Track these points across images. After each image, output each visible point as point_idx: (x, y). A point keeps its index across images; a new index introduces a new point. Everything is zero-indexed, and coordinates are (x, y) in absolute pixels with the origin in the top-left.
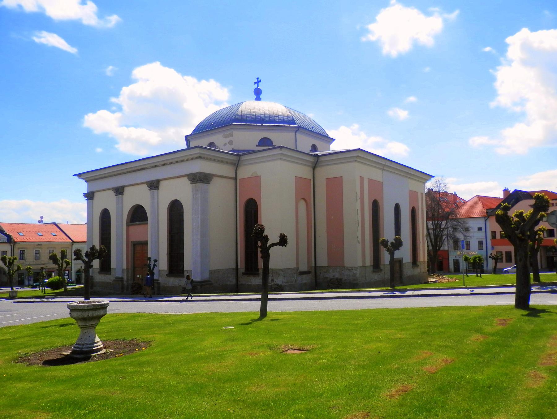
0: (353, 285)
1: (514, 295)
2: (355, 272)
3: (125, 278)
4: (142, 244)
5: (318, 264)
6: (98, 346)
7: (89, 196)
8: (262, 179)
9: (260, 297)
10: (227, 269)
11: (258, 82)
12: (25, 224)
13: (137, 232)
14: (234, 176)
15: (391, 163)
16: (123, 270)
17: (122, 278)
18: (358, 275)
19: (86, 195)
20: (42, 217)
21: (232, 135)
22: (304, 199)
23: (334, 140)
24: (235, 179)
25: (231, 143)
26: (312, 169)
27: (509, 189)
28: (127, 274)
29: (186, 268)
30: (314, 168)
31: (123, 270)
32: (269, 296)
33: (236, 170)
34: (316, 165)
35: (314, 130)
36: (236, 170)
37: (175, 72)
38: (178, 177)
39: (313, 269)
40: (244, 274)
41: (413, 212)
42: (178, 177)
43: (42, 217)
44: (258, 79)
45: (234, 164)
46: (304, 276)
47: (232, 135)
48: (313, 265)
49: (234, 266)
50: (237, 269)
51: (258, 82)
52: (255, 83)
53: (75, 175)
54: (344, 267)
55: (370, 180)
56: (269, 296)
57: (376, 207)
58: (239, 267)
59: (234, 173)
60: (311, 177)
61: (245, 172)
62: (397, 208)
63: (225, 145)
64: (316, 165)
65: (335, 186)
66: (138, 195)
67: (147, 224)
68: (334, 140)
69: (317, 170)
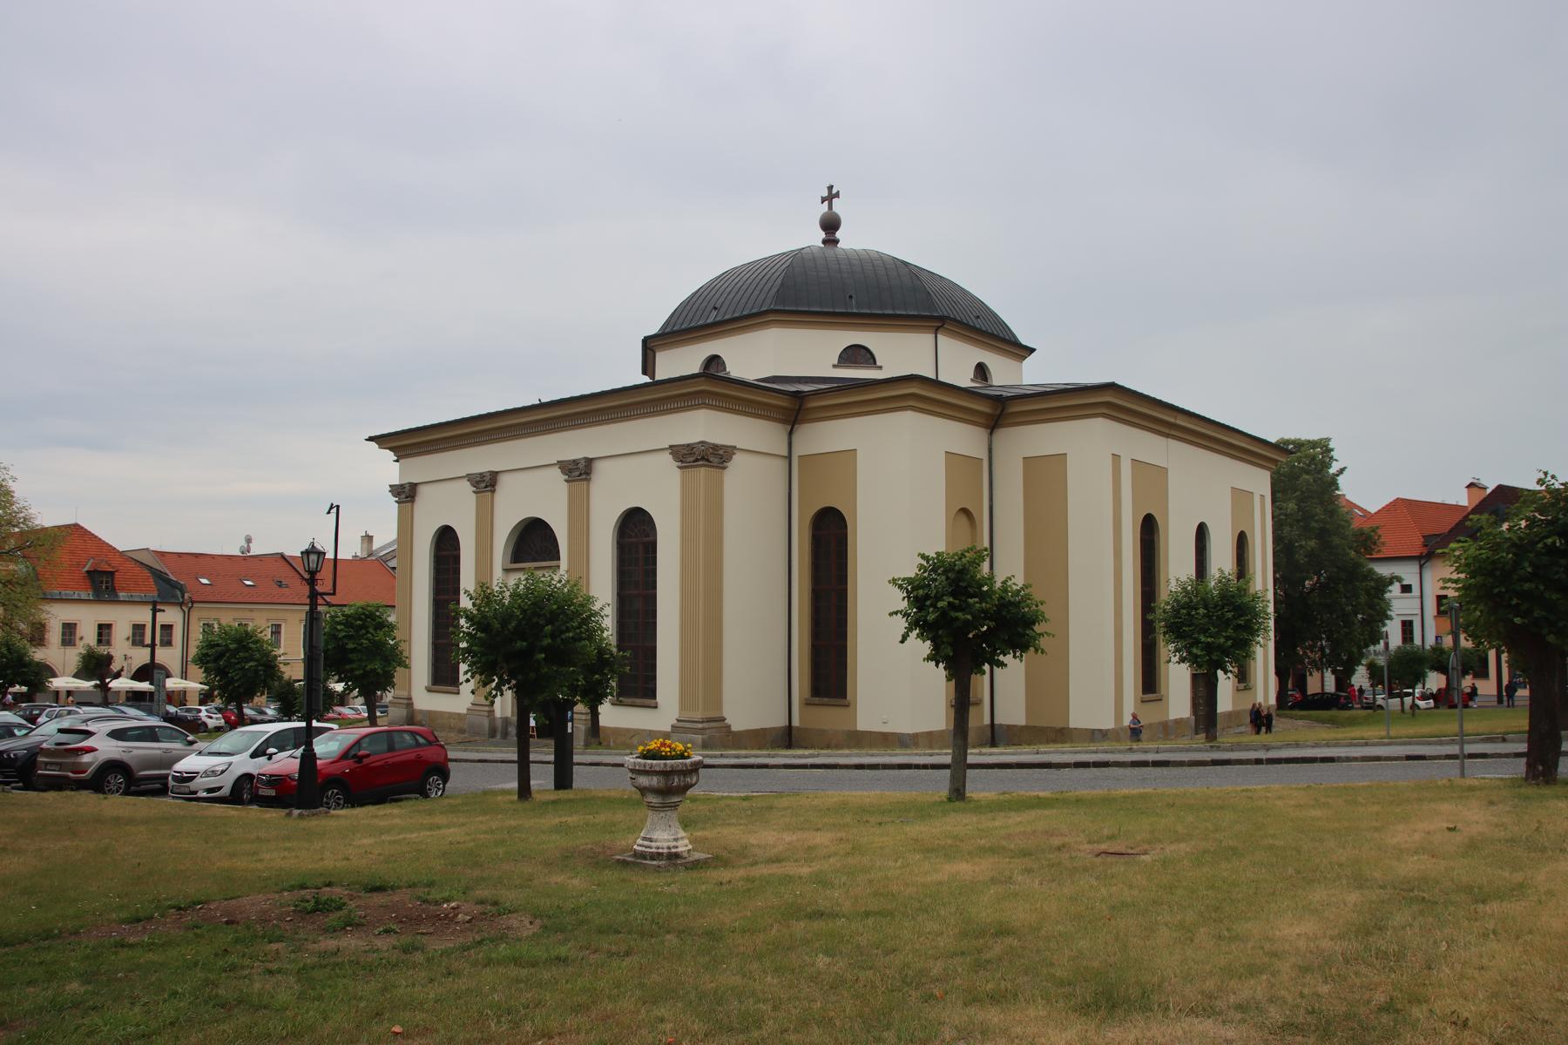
0: (838, 747)
1: (1524, 760)
6: (1242, 542)
7: (406, 494)
9: (948, 760)
11: (831, 196)
12: (213, 557)
19: (397, 490)
20: (249, 540)
23: (1032, 350)
24: (789, 457)
27: (1484, 482)
32: (971, 759)
33: (791, 433)
35: (978, 324)
36: (791, 433)
41: (1242, 542)
43: (249, 540)
44: (830, 188)
51: (831, 196)
53: (371, 439)
57: (1149, 529)
60: (984, 456)
62: (1202, 532)
68: (1032, 350)
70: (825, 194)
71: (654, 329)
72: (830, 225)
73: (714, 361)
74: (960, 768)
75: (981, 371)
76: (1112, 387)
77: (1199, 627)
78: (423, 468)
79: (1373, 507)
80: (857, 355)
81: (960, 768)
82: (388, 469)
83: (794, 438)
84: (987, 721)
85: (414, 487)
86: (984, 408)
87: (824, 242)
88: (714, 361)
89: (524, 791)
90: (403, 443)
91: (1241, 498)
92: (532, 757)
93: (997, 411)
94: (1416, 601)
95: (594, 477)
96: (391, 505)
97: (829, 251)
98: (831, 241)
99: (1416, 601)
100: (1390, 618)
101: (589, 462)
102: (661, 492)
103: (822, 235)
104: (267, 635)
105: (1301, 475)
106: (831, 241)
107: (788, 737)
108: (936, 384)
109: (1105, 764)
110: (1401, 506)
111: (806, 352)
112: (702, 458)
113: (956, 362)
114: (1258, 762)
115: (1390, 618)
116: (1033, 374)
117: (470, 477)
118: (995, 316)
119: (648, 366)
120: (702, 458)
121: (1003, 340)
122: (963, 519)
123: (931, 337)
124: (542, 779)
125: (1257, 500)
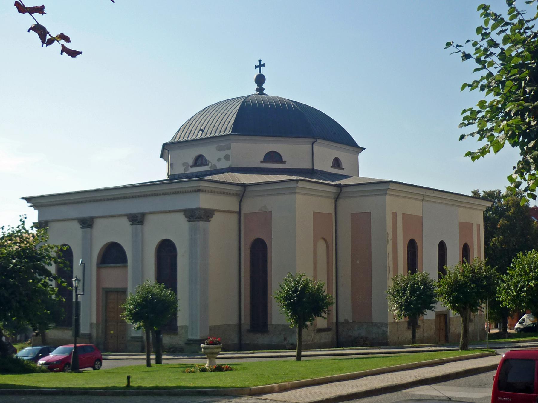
2: (385, 329)
3: (94, 335)
4: (118, 292)
5: (341, 319)
8: (273, 215)
9: (295, 354)
10: (228, 325)
11: (260, 66)
13: (112, 277)
14: (238, 210)
15: (432, 191)
16: (91, 324)
17: (142, 337)
18: (388, 333)
21: (229, 148)
22: (324, 239)
23: (364, 149)
24: (239, 213)
25: (227, 158)
26: (333, 201)
28: (97, 330)
29: (180, 323)
30: (336, 201)
31: (91, 324)
32: (303, 353)
34: (339, 195)
36: (240, 202)
37: (347, 402)
38: (170, 212)
39: (335, 325)
40: (249, 331)
42: (170, 212)
44: (260, 61)
45: (238, 195)
46: (323, 334)
47: (229, 148)
48: (335, 321)
49: (234, 320)
50: (240, 324)
51: (260, 66)
52: (256, 67)
53: (23, 198)
54: (372, 323)
55: (404, 215)
56: (303, 353)
57: (412, 248)
58: (243, 322)
59: (238, 206)
60: (332, 211)
61: (251, 206)
62: (442, 247)
63: (219, 160)
64: (339, 195)
65: (362, 223)
66: (120, 233)
67: (126, 267)
68: (364, 149)
69: (341, 202)
70: (258, 64)
72: (260, 80)
78: (52, 213)
83: (242, 204)
89: (149, 365)
91: (466, 228)
95: (146, 223)
98: (260, 90)
100: (431, 308)
101: (143, 215)
102: (178, 230)
103: (256, 86)
104: (495, 373)
106: (260, 90)
112: (195, 216)
120: (195, 216)
124: (153, 362)
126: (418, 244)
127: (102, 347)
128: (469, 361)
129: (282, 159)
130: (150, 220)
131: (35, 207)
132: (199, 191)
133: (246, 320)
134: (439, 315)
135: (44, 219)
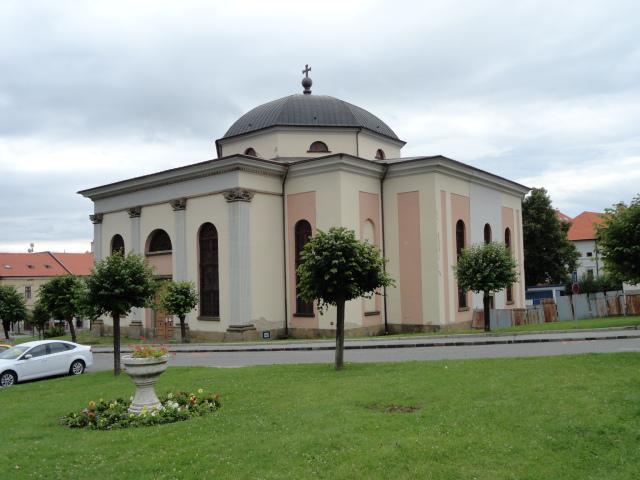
6: (507, 232)
11: (307, 70)
22: (369, 220)
23: (405, 143)
24: (283, 195)
26: (379, 181)
32: (346, 344)
40: (295, 316)
41: (507, 232)
42: (210, 194)
51: (307, 70)
53: (79, 192)
56: (346, 344)
57: (460, 226)
62: (487, 229)
66: (158, 217)
68: (405, 143)
69: (386, 182)
71: (221, 136)
72: (307, 84)
73: (250, 151)
74: (340, 348)
75: (380, 153)
76: (440, 157)
77: (481, 273)
79: (573, 216)
80: (318, 146)
81: (340, 348)
82: (89, 206)
84: (383, 322)
85: (102, 215)
86: (378, 169)
87: (305, 92)
88: (250, 151)
90: (97, 194)
91: (507, 212)
92: (122, 349)
93: (385, 171)
94: (590, 263)
96: (91, 224)
97: (307, 96)
98: (307, 92)
99: (590, 263)
100: (580, 255)
103: (303, 89)
105: (537, 209)
106: (307, 92)
107: (286, 334)
108: (357, 158)
109: (432, 345)
110: (585, 216)
111: (292, 146)
113: (368, 149)
114: (510, 342)
115: (580, 255)
116: (406, 153)
117: (126, 209)
118: (387, 127)
119: (219, 153)
120: (235, 196)
121: (391, 138)
122: (369, 224)
123: (354, 137)
125: (514, 212)
126: (466, 225)
127: (151, 334)
128: (141, 175)
129: (327, 148)
130: (190, 204)
131: (94, 199)
132: (238, 169)
133: (292, 308)
134: (214, 315)
135: (100, 211)
